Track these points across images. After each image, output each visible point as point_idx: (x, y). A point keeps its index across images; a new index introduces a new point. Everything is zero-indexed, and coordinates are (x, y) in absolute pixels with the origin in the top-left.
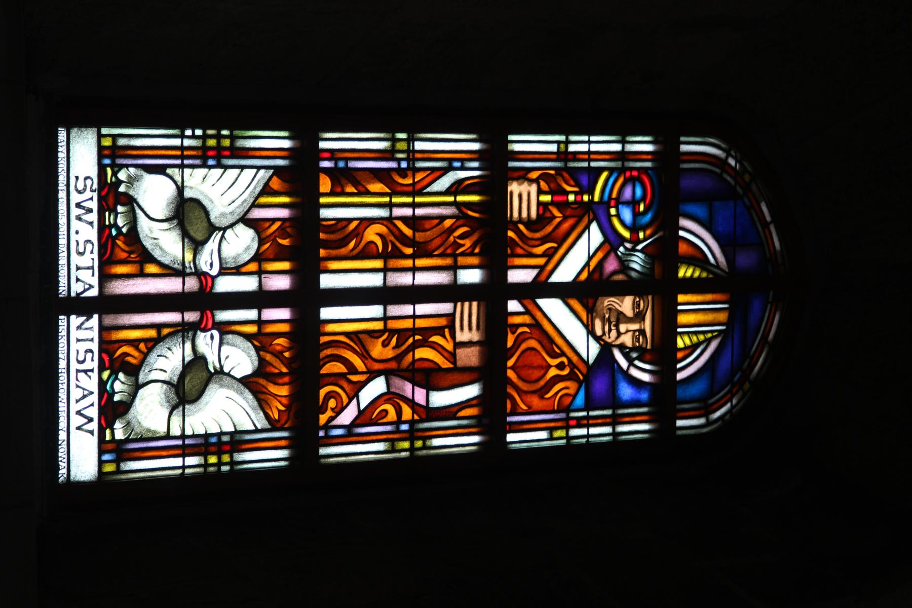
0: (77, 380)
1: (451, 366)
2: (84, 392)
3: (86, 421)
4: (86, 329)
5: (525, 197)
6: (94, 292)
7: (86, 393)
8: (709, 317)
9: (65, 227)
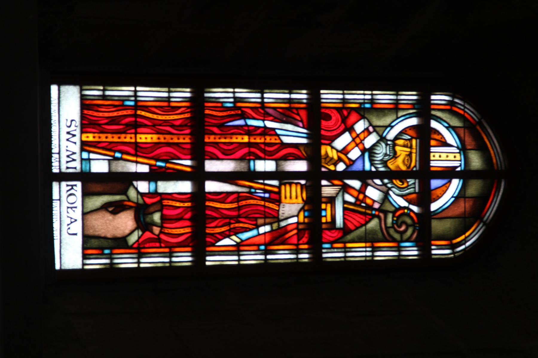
0: (68, 212)
1: (307, 232)
2: (71, 220)
3: (70, 140)
4: (70, 151)
5: (392, 163)
6: (78, 170)
7: (73, 220)
8: (499, 165)
9: (57, 101)
